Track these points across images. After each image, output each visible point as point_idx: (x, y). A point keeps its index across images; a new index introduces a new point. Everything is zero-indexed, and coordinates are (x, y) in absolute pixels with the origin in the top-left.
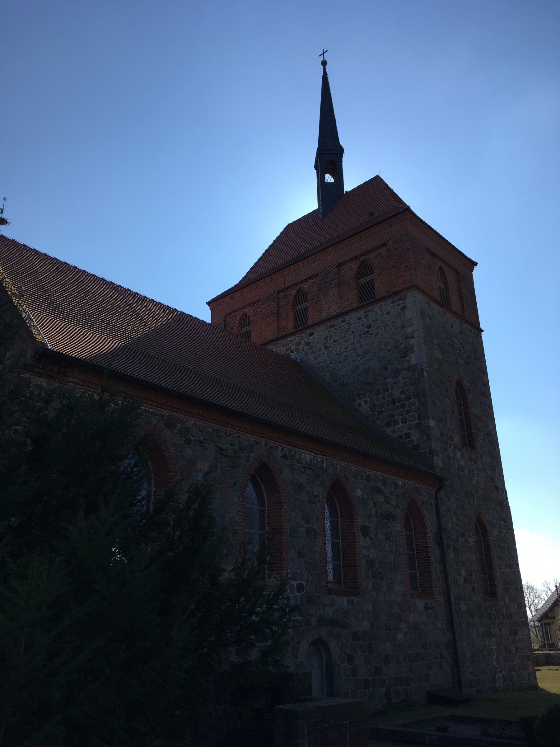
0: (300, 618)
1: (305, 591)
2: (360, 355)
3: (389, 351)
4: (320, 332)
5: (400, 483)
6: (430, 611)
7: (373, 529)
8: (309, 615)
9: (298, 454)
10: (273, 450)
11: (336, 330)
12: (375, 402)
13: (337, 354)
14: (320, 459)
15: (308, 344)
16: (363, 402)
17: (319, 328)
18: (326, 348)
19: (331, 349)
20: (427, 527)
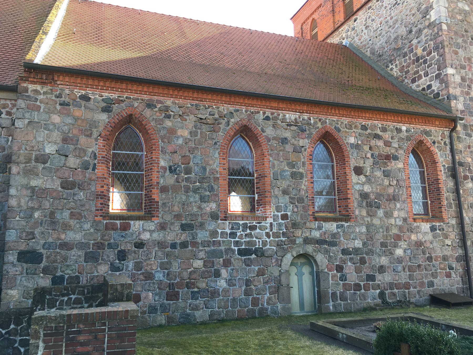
0: (284, 239)
1: (289, 219)
2: (391, 26)
3: (413, 15)
4: (361, 16)
5: (404, 128)
6: (438, 231)
7: (369, 169)
8: (294, 236)
9: (281, 115)
10: (254, 115)
11: (372, 11)
12: (403, 64)
13: (374, 31)
14: (306, 117)
15: (353, 29)
16: (395, 66)
17: (360, 13)
18: (367, 28)
19: (370, 28)
20: (437, 163)
